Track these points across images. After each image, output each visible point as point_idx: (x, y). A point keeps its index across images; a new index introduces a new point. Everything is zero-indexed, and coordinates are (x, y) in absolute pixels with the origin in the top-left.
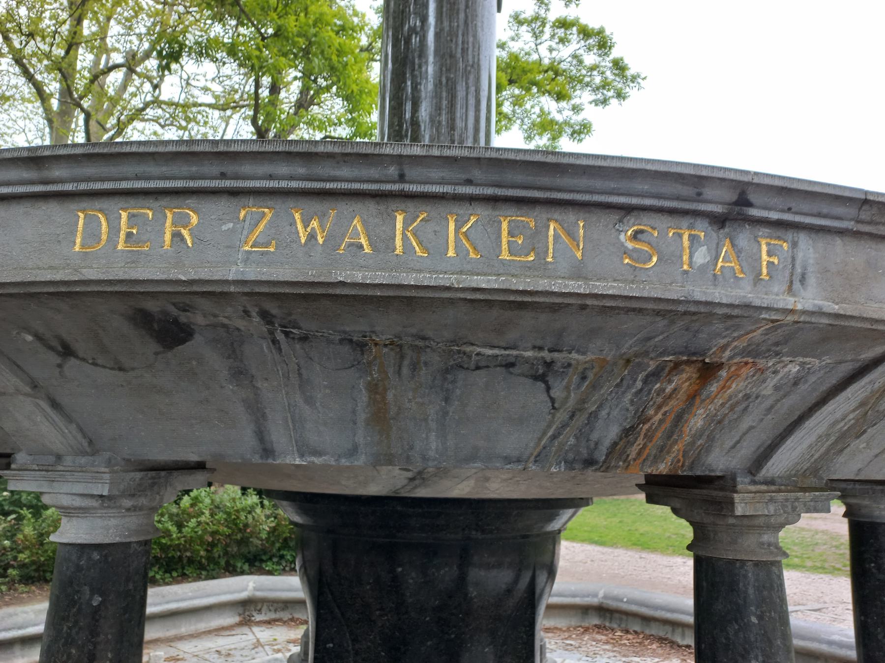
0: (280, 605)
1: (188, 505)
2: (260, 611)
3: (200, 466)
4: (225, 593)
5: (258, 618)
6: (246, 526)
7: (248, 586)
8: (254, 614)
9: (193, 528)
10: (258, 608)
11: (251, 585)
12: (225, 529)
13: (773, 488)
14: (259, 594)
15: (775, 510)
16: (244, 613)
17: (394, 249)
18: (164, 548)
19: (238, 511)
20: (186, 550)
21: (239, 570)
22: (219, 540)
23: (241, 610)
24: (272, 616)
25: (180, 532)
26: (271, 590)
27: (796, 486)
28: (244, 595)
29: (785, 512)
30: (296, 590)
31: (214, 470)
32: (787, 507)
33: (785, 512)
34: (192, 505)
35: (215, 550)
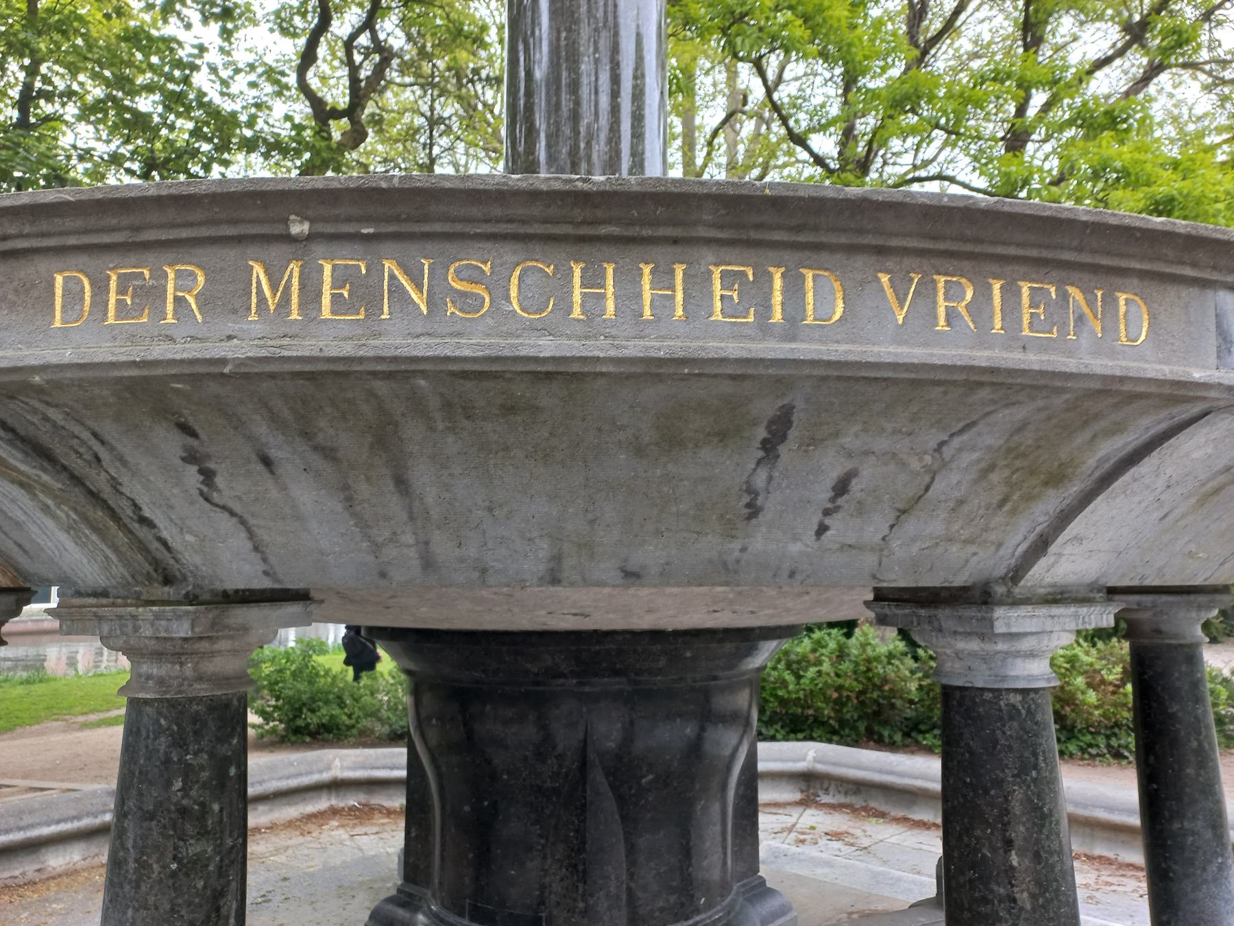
0: (850, 786)
1: (808, 649)
2: (827, 791)
3: (301, 596)
4: (775, 760)
5: (825, 799)
6: (885, 680)
7: (806, 754)
8: (820, 793)
9: (812, 680)
10: (826, 786)
11: (811, 755)
12: (855, 683)
13: (104, 601)
14: (820, 768)
15: (110, 631)
16: (808, 790)
17: (604, 312)
18: (783, 702)
19: (869, 661)
20: (809, 707)
21: (887, 740)
22: (848, 697)
23: (803, 785)
24: (841, 799)
25: (798, 683)
26: (834, 764)
27: (138, 598)
28: (801, 766)
29: (123, 633)
30: (933, 780)
31: (322, 601)
32: (127, 626)
33: (123, 633)
34: (814, 651)
35: (845, 710)
